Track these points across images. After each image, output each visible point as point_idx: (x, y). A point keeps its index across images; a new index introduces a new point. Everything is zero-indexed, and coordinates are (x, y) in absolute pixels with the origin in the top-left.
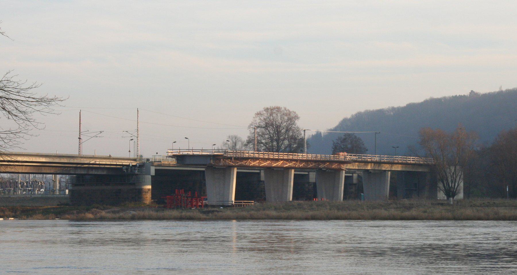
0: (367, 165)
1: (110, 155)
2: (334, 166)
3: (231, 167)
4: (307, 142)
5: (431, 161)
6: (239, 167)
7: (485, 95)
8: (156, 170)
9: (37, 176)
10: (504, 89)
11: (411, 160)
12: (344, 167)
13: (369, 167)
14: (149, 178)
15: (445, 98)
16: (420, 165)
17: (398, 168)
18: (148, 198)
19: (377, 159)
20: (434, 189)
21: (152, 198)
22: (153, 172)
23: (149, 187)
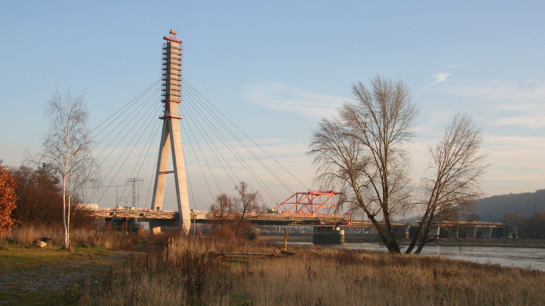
0: (483, 226)
1: (161, 118)
2: (473, 226)
3: (438, 226)
4: (468, 221)
5: (507, 224)
6: (440, 226)
7: (516, 195)
8: (410, 227)
9: (182, 151)
10: (524, 192)
11: (499, 224)
12: (476, 226)
13: (484, 226)
14: (408, 230)
15: (500, 195)
16: (503, 226)
17: (494, 227)
18: (408, 236)
19: (487, 223)
20: (507, 234)
21: (409, 236)
22: (409, 228)
23: (408, 233)
